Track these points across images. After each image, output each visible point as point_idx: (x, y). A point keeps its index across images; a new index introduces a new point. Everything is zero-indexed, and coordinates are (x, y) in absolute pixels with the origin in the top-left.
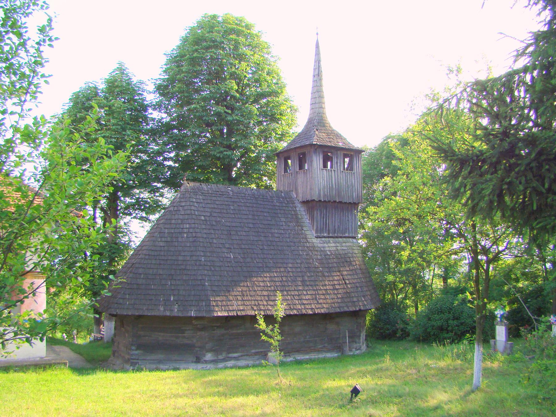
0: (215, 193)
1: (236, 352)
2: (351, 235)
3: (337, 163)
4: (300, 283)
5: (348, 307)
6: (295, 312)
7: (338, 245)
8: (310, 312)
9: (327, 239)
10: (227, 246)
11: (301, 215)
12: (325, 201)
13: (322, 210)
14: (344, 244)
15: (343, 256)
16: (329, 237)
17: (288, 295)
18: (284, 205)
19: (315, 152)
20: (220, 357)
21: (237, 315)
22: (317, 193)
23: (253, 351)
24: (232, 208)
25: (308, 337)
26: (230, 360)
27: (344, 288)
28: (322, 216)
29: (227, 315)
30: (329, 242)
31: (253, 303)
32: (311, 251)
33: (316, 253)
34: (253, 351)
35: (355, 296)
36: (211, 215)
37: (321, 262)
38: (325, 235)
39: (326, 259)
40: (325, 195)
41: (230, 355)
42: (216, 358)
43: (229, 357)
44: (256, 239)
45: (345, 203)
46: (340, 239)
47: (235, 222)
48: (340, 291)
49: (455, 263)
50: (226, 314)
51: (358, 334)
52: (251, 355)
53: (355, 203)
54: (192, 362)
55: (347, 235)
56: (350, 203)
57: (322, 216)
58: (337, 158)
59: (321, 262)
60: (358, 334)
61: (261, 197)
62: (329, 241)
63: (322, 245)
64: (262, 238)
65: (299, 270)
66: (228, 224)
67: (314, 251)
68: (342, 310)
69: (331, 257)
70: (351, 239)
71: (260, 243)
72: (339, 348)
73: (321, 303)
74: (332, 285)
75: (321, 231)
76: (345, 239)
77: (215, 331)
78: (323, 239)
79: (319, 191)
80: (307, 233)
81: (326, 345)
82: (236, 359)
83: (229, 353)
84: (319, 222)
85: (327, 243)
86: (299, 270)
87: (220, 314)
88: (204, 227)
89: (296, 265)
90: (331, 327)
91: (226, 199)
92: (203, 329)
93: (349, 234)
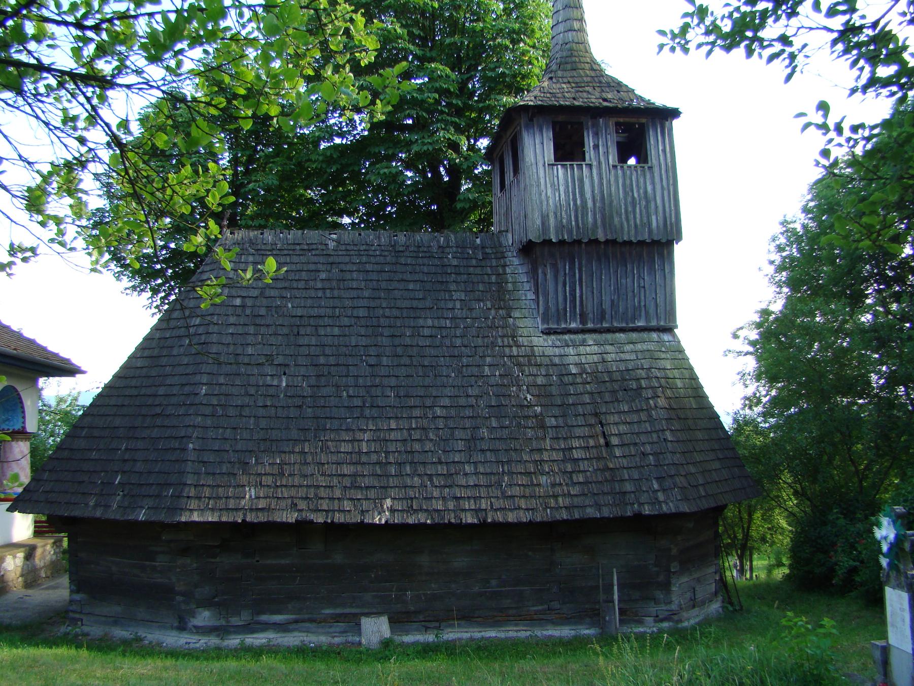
0: (292, 247)
1: (280, 613)
2: (654, 323)
3: (596, 147)
4: (461, 445)
5: (598, 506)
6: (422, 518)
7: (609, 348)
8: (470, 519)
9: (580, 336)
10: (280, 360)
11: (514, 283)
12: (562, 242)
13: (560, 265)
14: (628, 347)
15: (616, 376)
16: (583, 331)
17: (411, 476)
18: (474, 262)
19: (529, 126)
20: (235, 621)
21: (244, 521)
22: (538, 222)
23: (328, 611)
24: (323, 276)
25: (494, 582)
26: (263, 630)
27: (599, 458)
28: (561, 279)
29: (216, 519)
30: (583, 343)
31: (302, 492)
32: (519, 365)
33: (534, 370)
34: (328, 611)
35: (631, 479)
36: (262, 293)
37: (543, 393)
38: (573, 325)
39: (563, 384)
40: (560, 227)
41: (264, 618)
42: (223, 623)
43: (259, 623)
44: (363, 341)
45: (629, 243)
46: (622, 336)
47: (319, 307)
48: (583, 465)
50: (211, 518)
51: (661, 578)
52: (325, 621)
54: (172, 628)
55: (641, 323)
56: (641, 243)
57: (561, 279)
58: (596, 135)
59: (543, 393)
60: (661, 578)
61: (412, 249)
62: (584, 340)
63: (557, 351)
64: (385, 341)
65: (468, 412)
66: (299, 312)
67: (530, 364)
68: (577, 516)
69: (579, 380)
70: (654, 335)
71: (373, 351)
72: (593, 614)
73: (512, 497)
74: (563, 450)
75: (560, 316)
76: (634, 336)
77: (218, 559)
78: (567, 337)
79: (545, 218)
80: (520, 323)
81: (556, 605)
82: (282, 627)
83: (259, 613)
84: (551, 295)
86: (468, 412)
87: (196, 517)
88: (232, 320)
89: (462, 401)
90: (569, 560)
91: (315, 259)
92: (185, 551)
93: (648, 319)
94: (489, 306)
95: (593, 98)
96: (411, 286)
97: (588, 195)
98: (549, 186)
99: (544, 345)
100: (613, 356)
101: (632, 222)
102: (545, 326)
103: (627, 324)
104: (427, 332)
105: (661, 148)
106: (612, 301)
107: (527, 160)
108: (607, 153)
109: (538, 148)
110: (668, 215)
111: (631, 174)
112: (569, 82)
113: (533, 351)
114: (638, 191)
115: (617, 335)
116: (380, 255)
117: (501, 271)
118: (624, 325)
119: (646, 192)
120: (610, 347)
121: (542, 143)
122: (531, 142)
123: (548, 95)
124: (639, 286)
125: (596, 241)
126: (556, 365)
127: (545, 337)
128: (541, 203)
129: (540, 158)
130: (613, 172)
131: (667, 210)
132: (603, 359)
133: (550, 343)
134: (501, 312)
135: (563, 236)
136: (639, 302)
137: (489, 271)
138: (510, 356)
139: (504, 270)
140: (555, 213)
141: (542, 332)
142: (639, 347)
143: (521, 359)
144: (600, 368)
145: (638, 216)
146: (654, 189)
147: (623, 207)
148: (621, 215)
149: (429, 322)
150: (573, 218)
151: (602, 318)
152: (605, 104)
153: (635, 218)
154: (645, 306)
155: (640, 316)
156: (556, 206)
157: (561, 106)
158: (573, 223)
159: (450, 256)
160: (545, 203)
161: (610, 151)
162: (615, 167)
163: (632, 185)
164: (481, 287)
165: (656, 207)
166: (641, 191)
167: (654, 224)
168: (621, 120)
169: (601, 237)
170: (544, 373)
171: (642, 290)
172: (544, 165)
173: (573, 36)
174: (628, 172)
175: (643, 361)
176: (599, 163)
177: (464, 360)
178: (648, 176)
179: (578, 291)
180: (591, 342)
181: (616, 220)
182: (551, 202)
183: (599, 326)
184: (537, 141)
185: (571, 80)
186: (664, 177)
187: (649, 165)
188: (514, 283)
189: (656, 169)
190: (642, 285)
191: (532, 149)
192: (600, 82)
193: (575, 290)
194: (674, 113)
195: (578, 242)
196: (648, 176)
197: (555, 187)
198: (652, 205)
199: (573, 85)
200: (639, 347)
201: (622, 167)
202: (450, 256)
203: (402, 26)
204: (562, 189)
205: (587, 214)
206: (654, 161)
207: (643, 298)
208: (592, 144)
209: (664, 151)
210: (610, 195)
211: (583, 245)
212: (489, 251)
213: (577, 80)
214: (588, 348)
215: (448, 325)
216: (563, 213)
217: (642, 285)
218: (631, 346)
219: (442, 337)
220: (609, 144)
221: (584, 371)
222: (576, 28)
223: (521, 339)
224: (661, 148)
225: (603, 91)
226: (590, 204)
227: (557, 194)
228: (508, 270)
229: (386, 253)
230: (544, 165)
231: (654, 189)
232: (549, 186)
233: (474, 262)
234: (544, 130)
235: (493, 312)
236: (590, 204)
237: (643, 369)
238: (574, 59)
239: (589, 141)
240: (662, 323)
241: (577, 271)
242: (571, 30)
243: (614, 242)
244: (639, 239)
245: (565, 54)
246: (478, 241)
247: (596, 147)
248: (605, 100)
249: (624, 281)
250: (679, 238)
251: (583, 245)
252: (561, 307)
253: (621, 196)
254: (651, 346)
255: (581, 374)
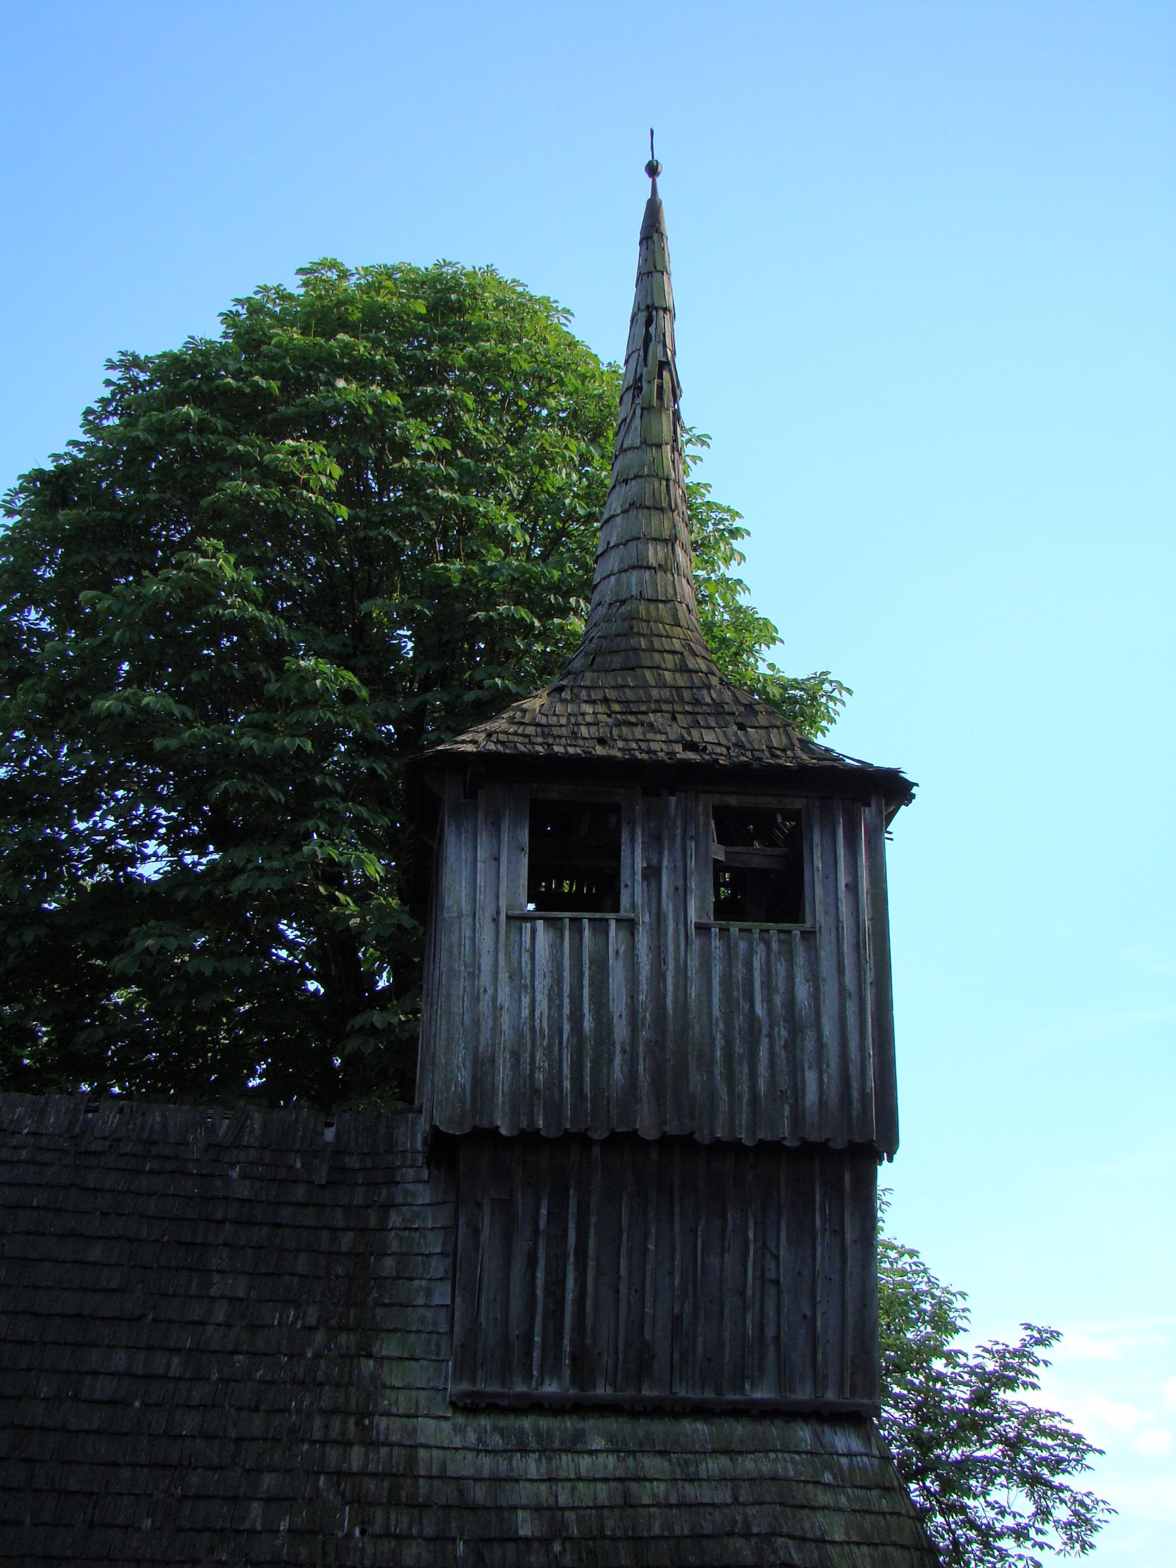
2: (804, 1393)
3: (652, 873)
7: (651, 1464)
9: (569, 1423)
12: (528, 1139)
14: (712, 1465)
16: (580, 1408)
22: (463, 1077)
30: (575, 1445)
33: (401, 1521)
38: (551, 1388)
45: (734, 1147)
46: (698, 1429)
49: (981, 1397)
53: (811, 1151)
55: (761, 1394)
56: (770, 1150)
58: (655, 840)
63: (487, 1464)
70: (804, 1434)
76: (739, 1429)
78: (526, 1423)
79: (482, 1066)
85: (546, 1450)
93: (785, 1379)
94: (312, 1320)
95: (662, 740)
96: (95, 1253)
97: (618, 1005)
98: (503, 976)
99: (447, 1441)
100: (661, 1488)
101: (744, 1087)
102: (465, 1386)
103: (719, 1391)
104: (103, 1388)
105: (842, 880)
106: (677, 1320)
107: (448, 902)
108: (681, 893)
109: (485, 876)
110: (854, 1070)
111: (751, 950)
112: (606, 701)
113: (412, 1461)
114: (768, 1000)
115: (687, 1425)
116: (29, 1162)
117: (373, 1221)
118: (709, 1394)
119: (791, 1001)
120: (657, 1460)
121: (497, 859)
122: (466, 854)
123: (530, 730)
124: (762, 1278)
125: (633, 1137)
126: (474, 1508)
127: (460, 1419)
128: (477, 1023)
129: (484, 898)
130: (696, 944)
131: (854, 1054)
132: (626, 1494)
133: (472, 1438)
134: (343, 1338)
135: (532, 1121)
136: (761, 1328)
137: (339, 1218)
138: (339, 1473)
139: (385, 1219)
140: (516, 1055)
141: (453, 1405)
142: (748, 1464)
143: (371, 1485)
144: (610, 1523)
145: (763, 1069)
146: (816, 996)
147: (719, 1043)
148: (712, 1064)
149: (120, 1360)
150: (566, 1071)
151: (642, 1369)
152: (691, 755)
153: (753, 1075)
154: (777, 1338)
155: (762, 1369)
156: (521, 1035)
157: (552, 757)
158: (567, 1084)
159: (235, 1173)
160: (487, 1025)
161: (693, 884)
162: (702, 929)
163: (749, 980)
164: (302, 1265)
165: (820, 1045)
166: (778, 1000)
167: (811, 1095)
168: (733, 801)
169: (646, 1124)
170: (429, 1531)
171: (771, 1290)
172: (496, 920)
173: (641, 582)
174: (742, 946)
175: (751, 1511)
176: (659, 918)
177: (194, 1479)
178: (801, 958)
179: (570, 1283)
180: (598, 1443)
181: (696, 1079)
182: (506, 1020)
183: (630, 1393)
184: (481, 854)
185: (611, 694)
186: (849, 962)
187: (808, 925)
188: (403, 1257)
189: (826, 941)
190: (771, 1275)
191: (465, 872)
192: (697, 702)
193: (562, 1282)
194: (891, 789)
195: (579, 1140)
196: (801, 958)
197: (522, 983)
198: (810, 1044)
199: (616, 707)
200: (748, 1464)
201: (724, 931)
202: (235, 1173)
203: (244, 561)
204: (542, 986)
205: (611, 1060)
206: (820, 917)
207: (771, 1314)
208: (639, 865)
209: (853, 887)
210: (683, 1007)
211: (596, 1150)
212: (351, 1162)
213: (630, 694)
214: (585, 1462)
215: (175, 1369)
216: (539, 1055)
217: (771, 1275)
218: (724, 1460)
219: (146, 1405)
220: (692, 864)
221: (557, 1531)
222: (652, 561)
223: (383, 1422)
224: (842, 880)
225: (697, 725)
226: (621, 1031)
227: (526, 1001)
228: (395, 1219)
229: (48, 1157)
230: (496, 920)
231: (816, 996)
232: (503, 976)
233: (300, 1193)
234: (505, 826)
235: (319, 1337)
236: (621, 1031)
237: (747, 1535)
238: (633, 642)
239: (634, 859)
240: (830, 1396)
241: (572, 1226)
242: (641, 566)
243: (687, 1143)
244: (762, 1135)
245: (613, 628)
246: (330, 1134)
247: (652, 873)
248: (690, 746)
249: (714, 1260)
250: (881, 1139)
251: (596, 1150)
252: (515, 1331)
253: (716, 1012)
254: (786, 1466)
255: (546, 1541)
